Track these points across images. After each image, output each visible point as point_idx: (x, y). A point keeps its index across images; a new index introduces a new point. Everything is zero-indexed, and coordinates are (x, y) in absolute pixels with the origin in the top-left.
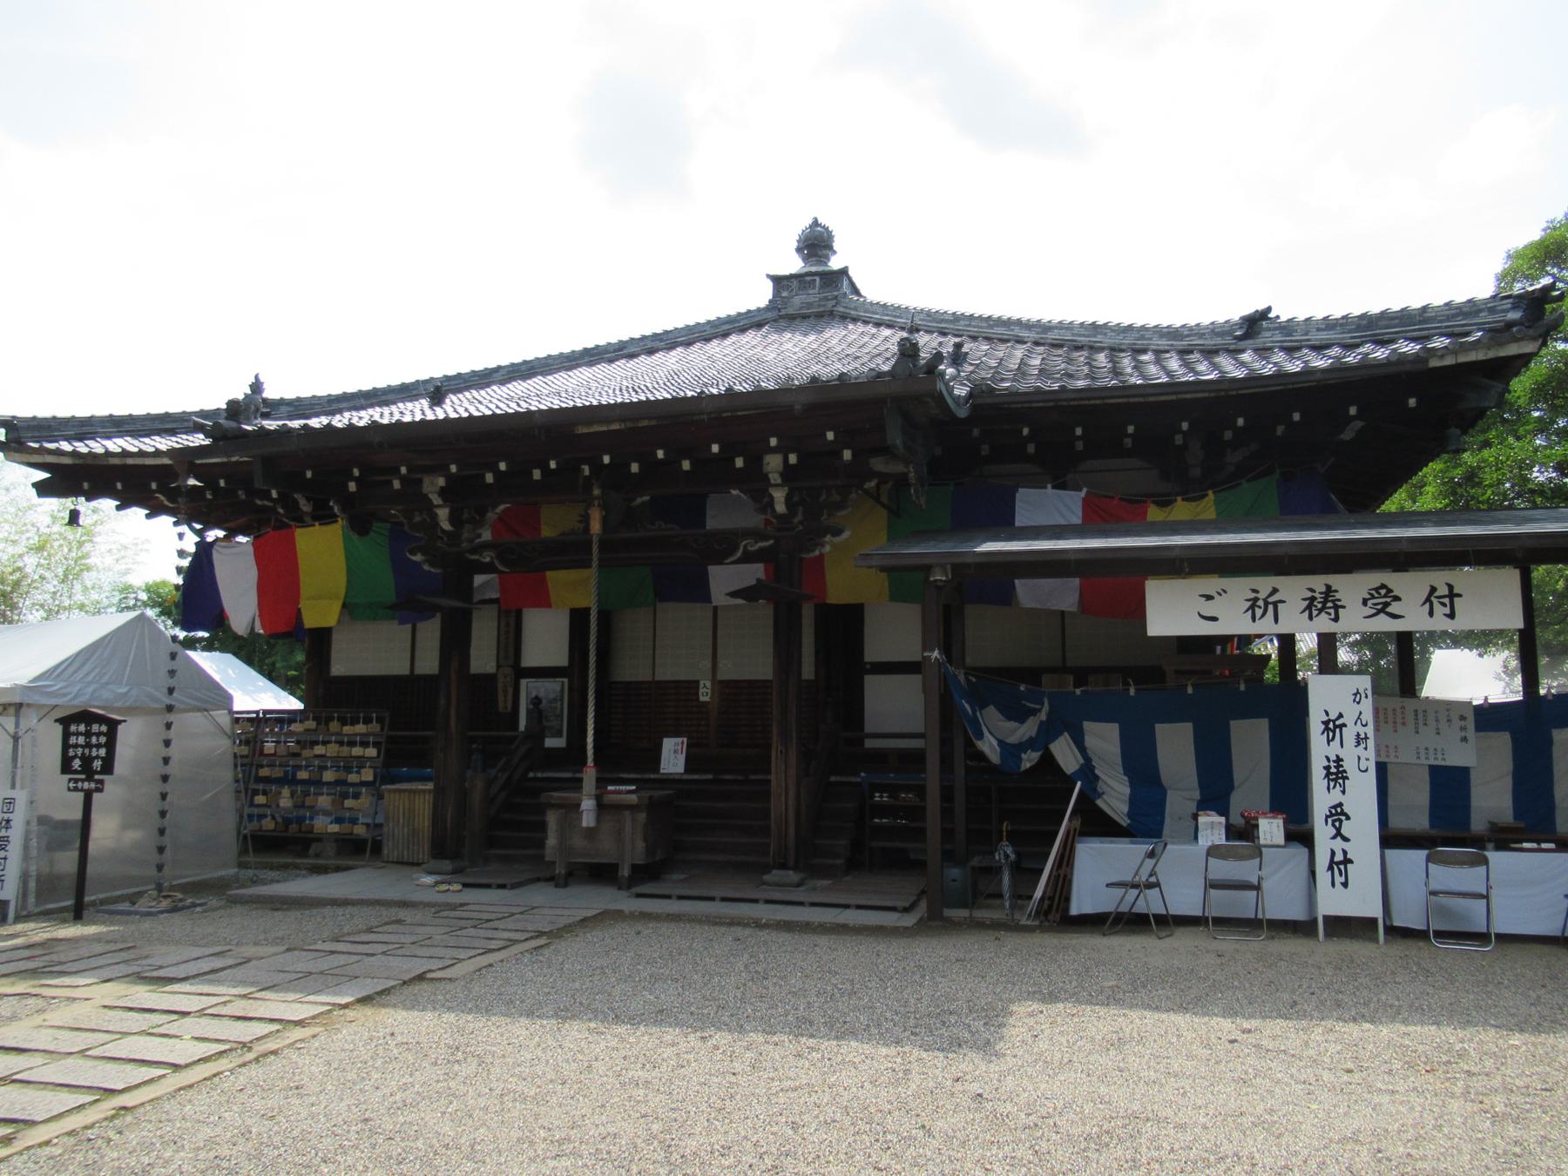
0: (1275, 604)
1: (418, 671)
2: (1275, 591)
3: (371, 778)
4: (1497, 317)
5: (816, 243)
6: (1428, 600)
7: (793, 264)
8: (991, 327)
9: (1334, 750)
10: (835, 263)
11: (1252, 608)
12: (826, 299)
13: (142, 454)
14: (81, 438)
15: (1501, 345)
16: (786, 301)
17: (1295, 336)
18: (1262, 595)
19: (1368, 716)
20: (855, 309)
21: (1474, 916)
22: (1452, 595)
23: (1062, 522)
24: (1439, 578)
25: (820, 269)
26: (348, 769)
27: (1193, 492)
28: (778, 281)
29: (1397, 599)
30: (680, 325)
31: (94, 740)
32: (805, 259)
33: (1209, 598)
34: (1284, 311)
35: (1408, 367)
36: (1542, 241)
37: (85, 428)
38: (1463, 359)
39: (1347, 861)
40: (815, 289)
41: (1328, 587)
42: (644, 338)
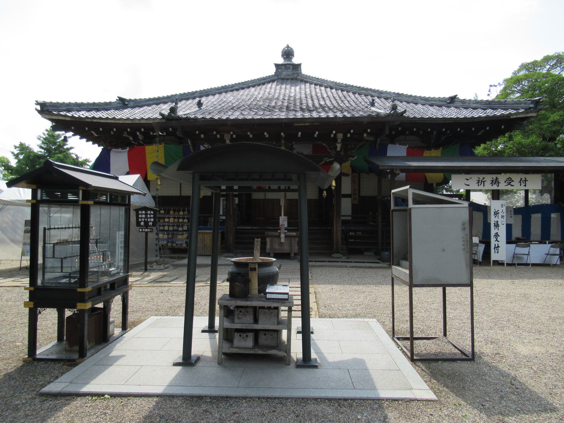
0: (484, 182)
1: (182, 195)
2: (484, 178)
3: (186, 229)
4: (526, 106)
5: (288, 54)
6: (520, 182)
7: (281, 61)
8: (360, 90)
9: (496, 219)
10: (295, 61)
11: (478, 183)
12: (294, 73)
13: (100, 118)
14: (69, 111)
15: (527, 113)
16: (280, 73)
17: (466, 104)
18: (481, 179)
19: (504, 211)
20: (306, 78)
21: (525, 260)
22: (526, 181)
23: (401, 155)
24: (523, 176)
25: (289, 63)
26: (178, 226)
27: (437, 147)
28: (277, 66)
29: (513, 181)
30: (250, 80)
31: (149, 216)
32: (284, 59)
33: (468, 180)
34: (461, 97)
35: (505, 118)
36: (511, 78)
37: (69, 107)
38: (518, 116)
39: (498, 247)
40: (288, 71)
41: (497, 178)
42: (239, 83)
